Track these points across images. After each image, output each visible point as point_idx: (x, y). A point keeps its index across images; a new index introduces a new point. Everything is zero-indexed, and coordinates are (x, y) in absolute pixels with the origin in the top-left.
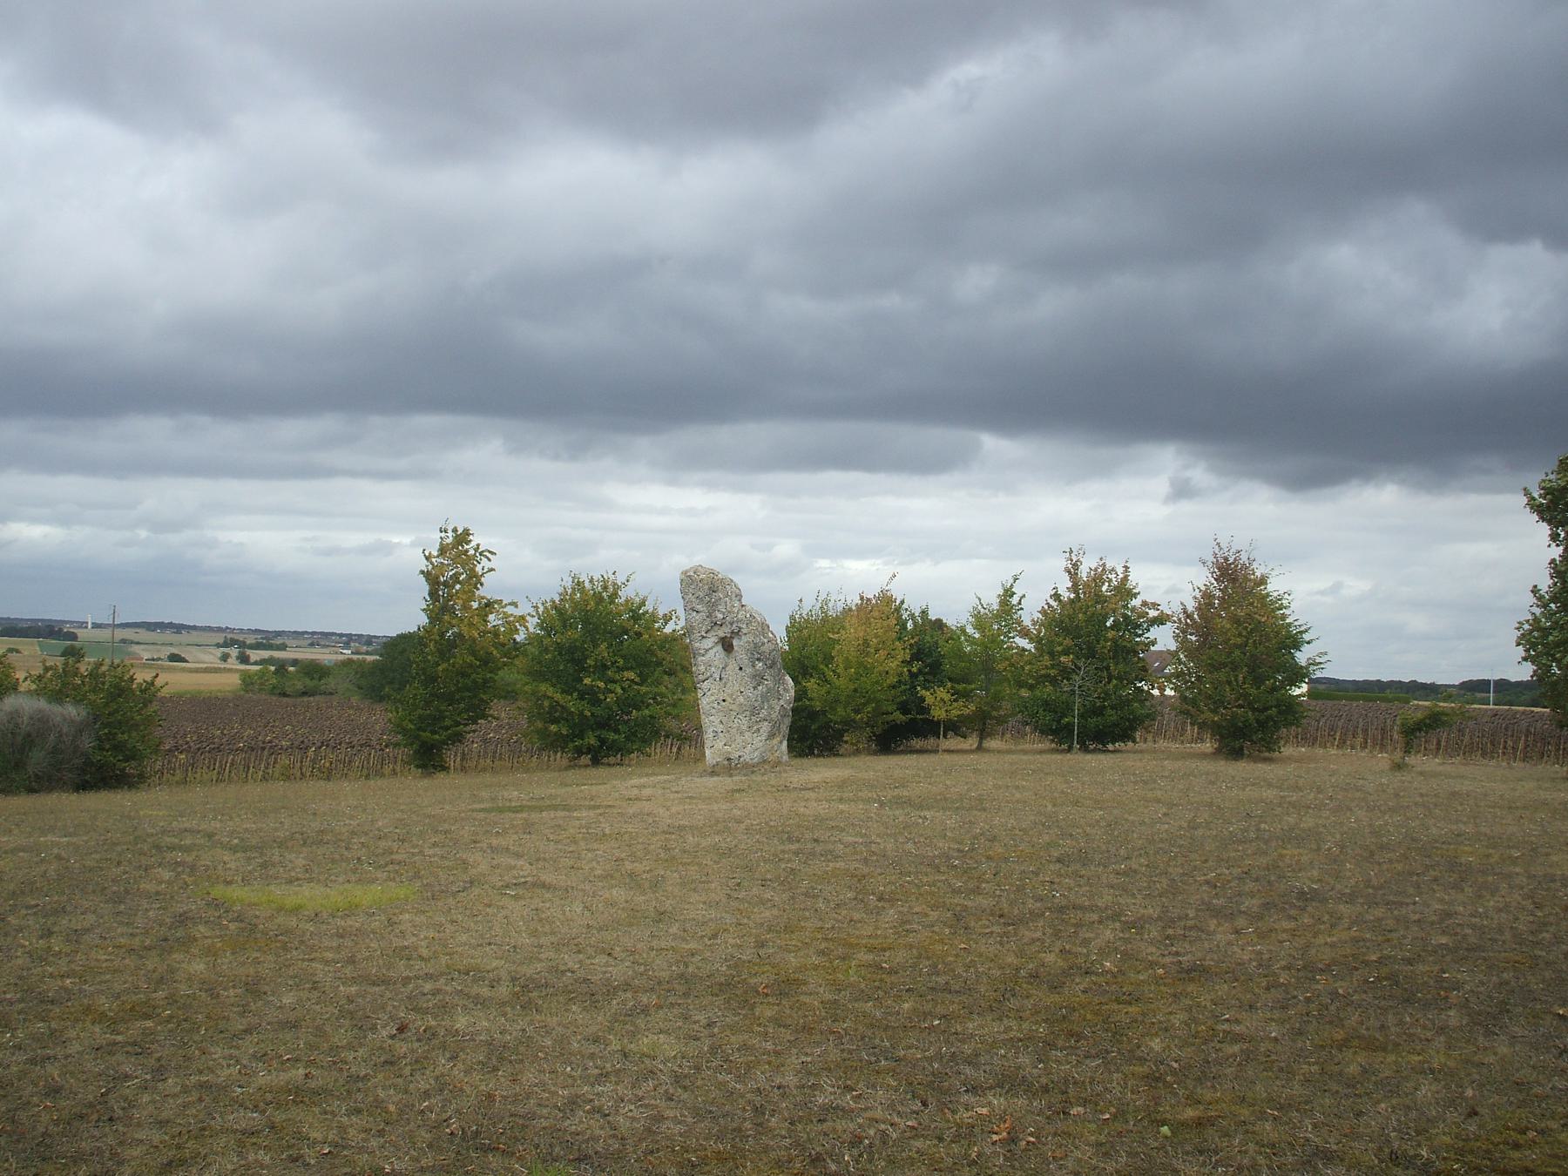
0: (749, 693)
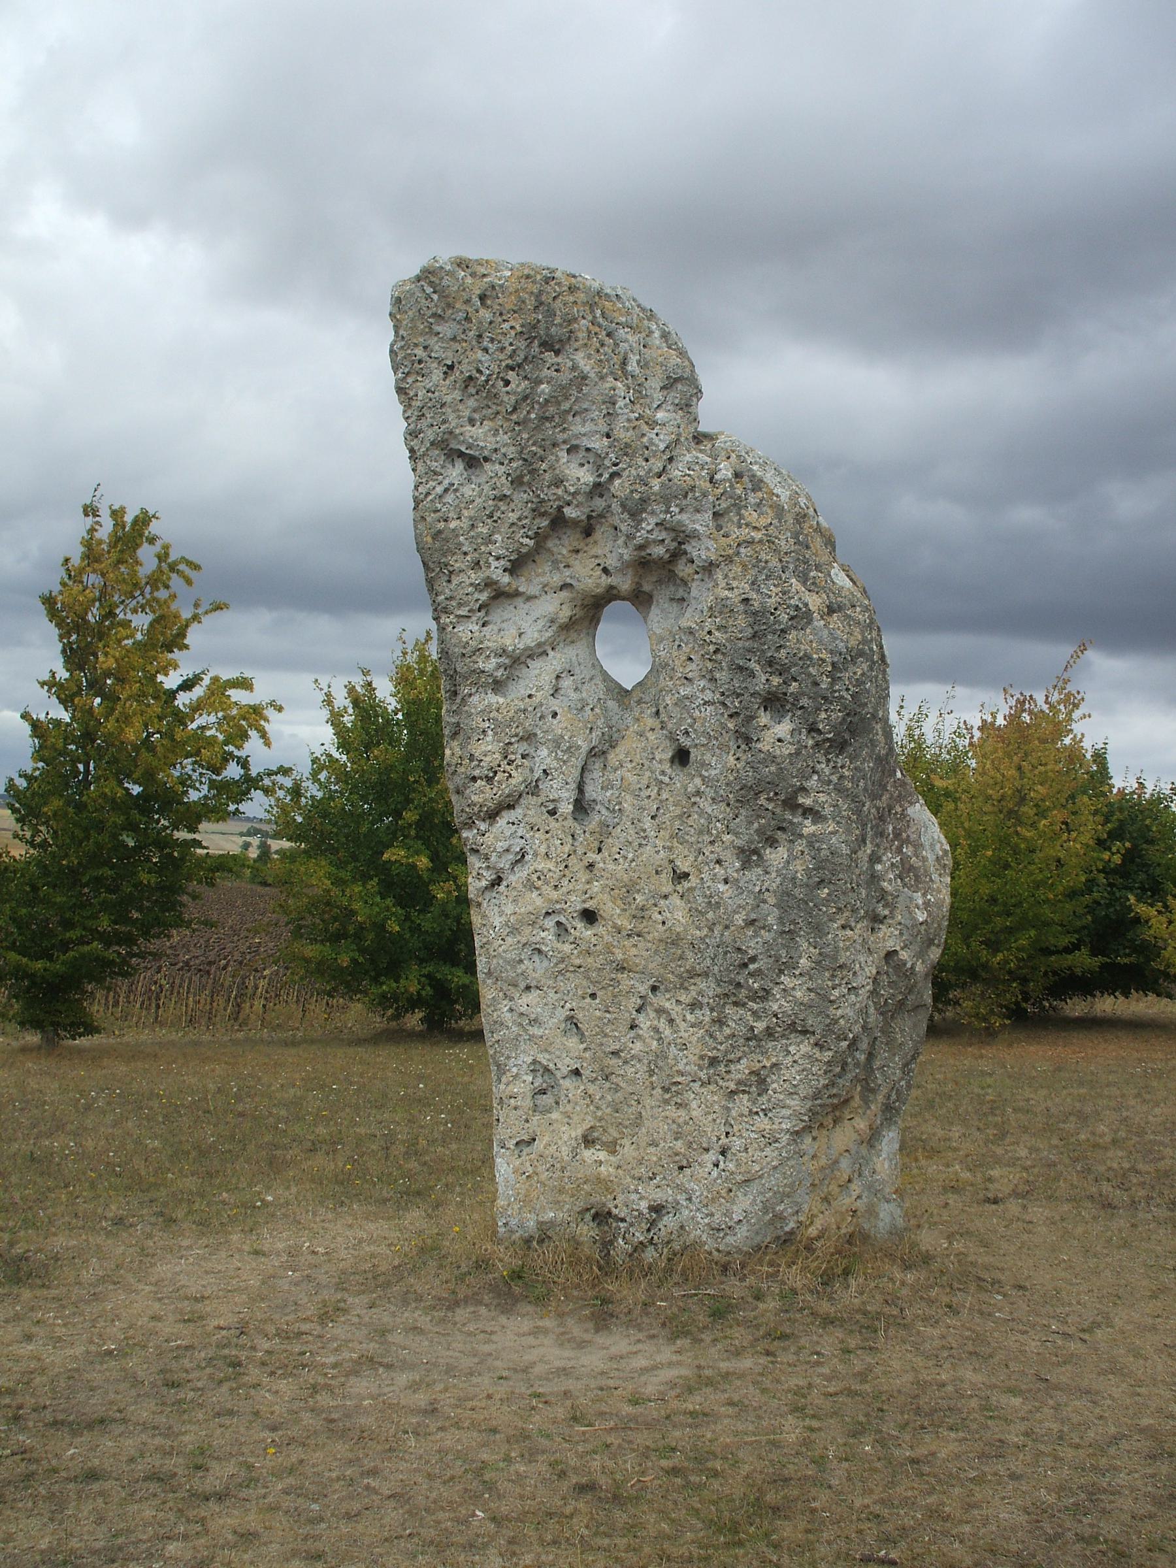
0: (721, 881)
